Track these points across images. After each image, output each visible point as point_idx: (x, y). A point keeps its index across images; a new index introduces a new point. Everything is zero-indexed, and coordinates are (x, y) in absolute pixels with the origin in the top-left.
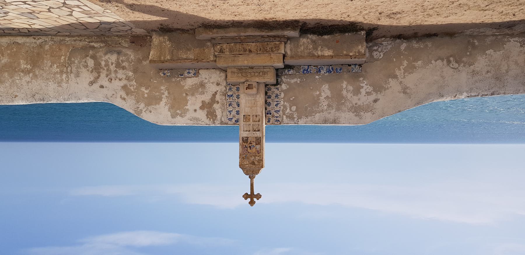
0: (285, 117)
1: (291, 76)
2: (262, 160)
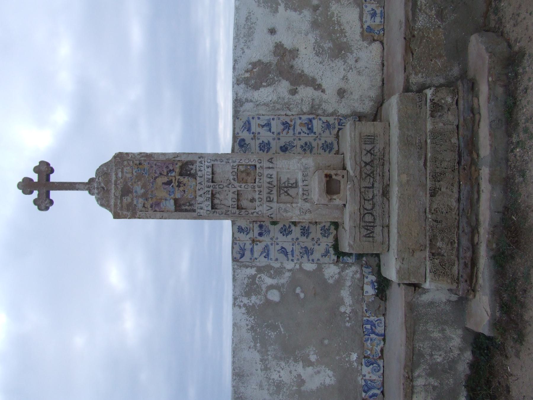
0: (253, 271)
2: (134, 216)
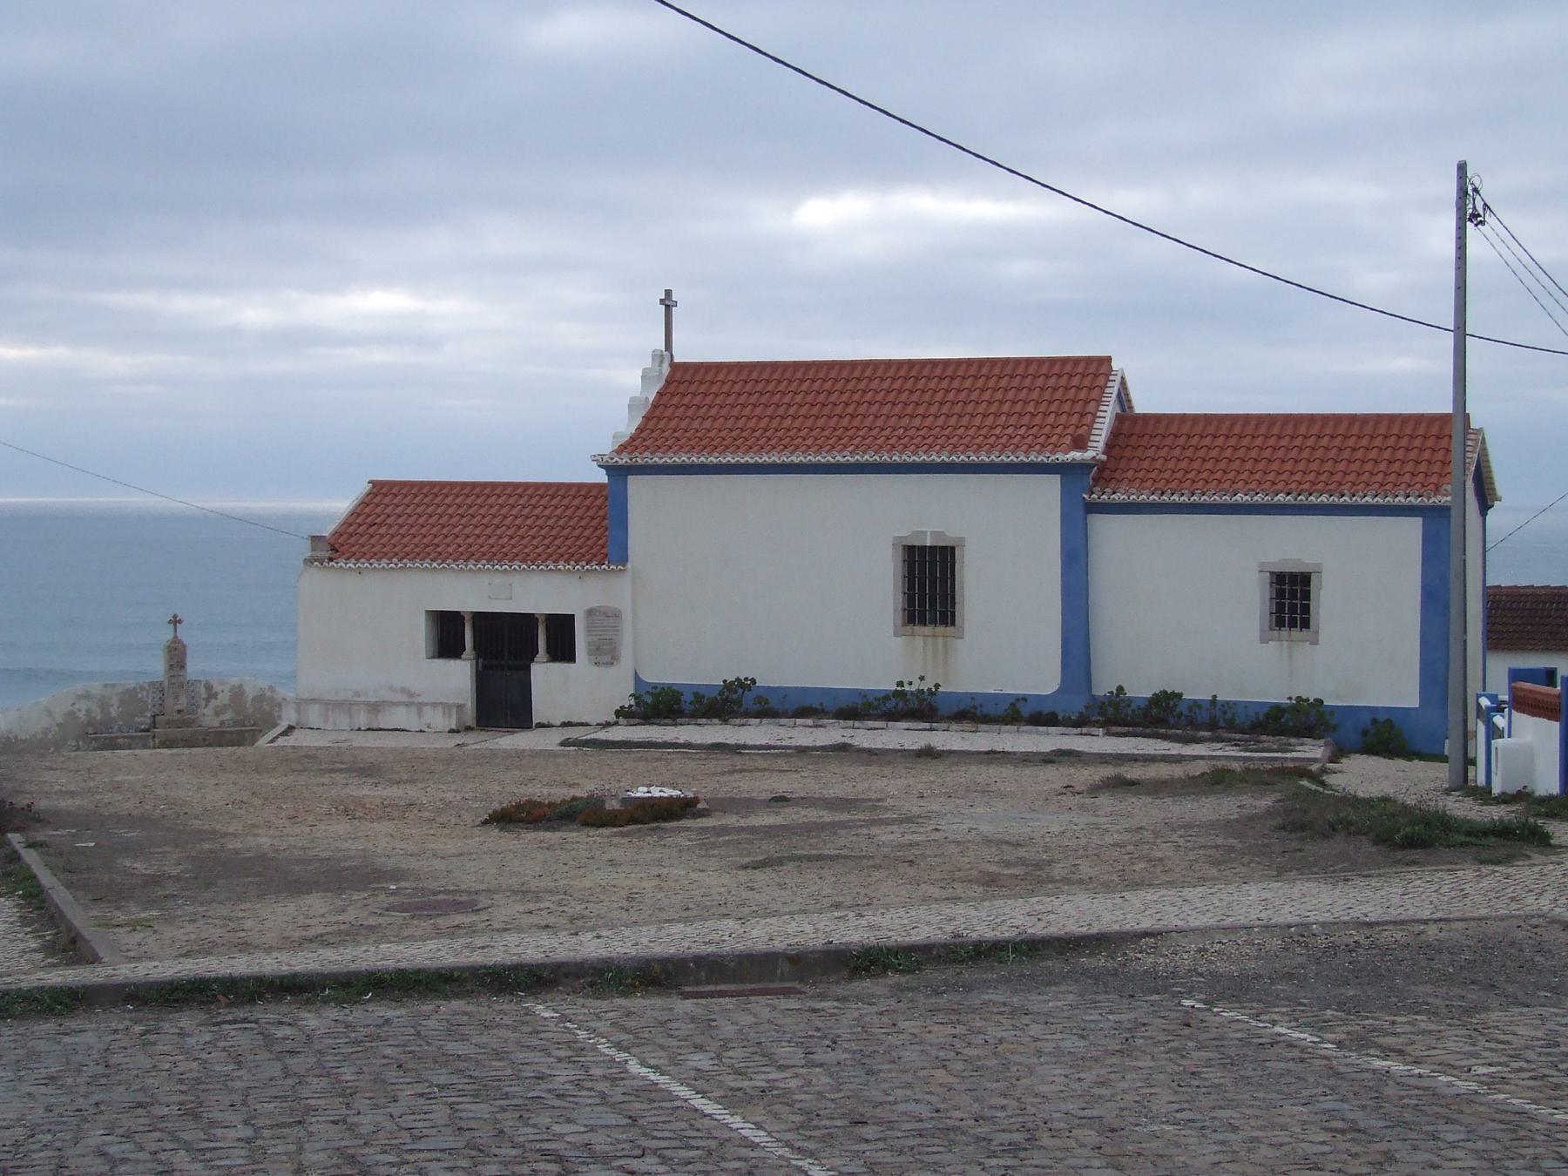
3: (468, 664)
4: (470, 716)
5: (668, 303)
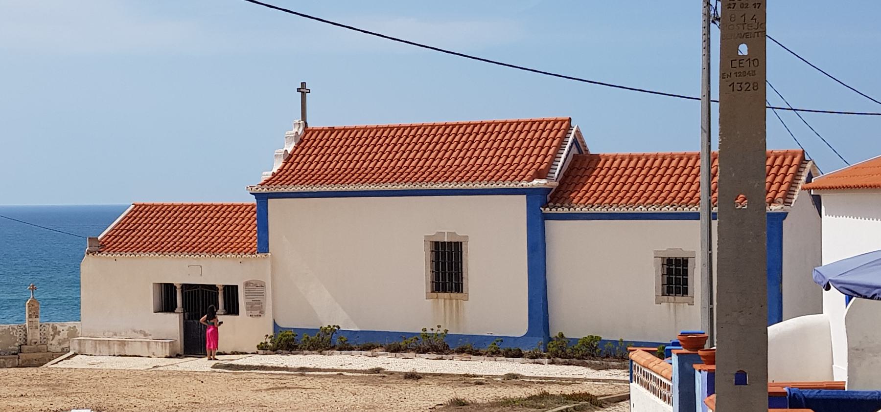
1: (13, 350)
3: (178, 315)
4: (179, 346)
5: (303, 90)
